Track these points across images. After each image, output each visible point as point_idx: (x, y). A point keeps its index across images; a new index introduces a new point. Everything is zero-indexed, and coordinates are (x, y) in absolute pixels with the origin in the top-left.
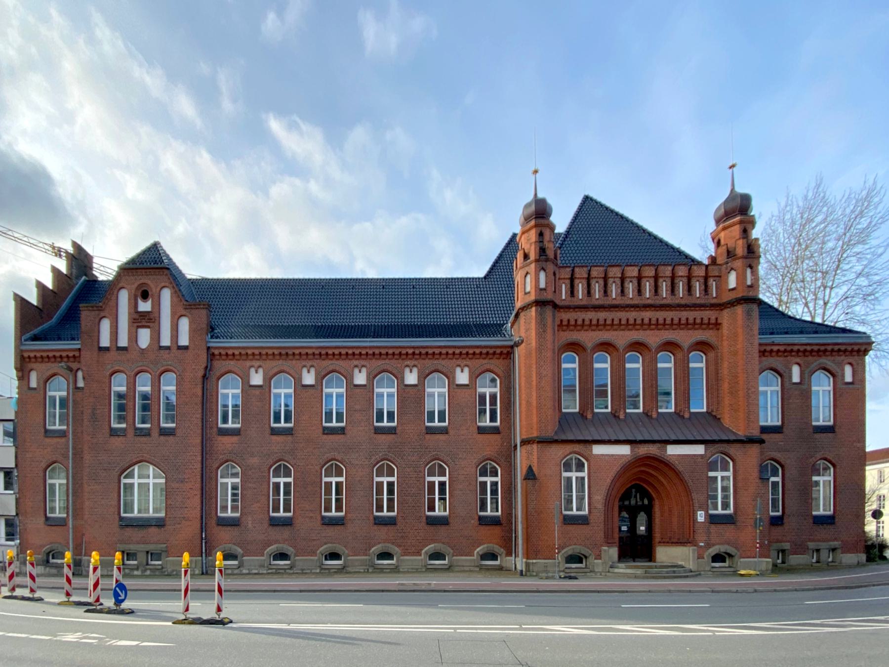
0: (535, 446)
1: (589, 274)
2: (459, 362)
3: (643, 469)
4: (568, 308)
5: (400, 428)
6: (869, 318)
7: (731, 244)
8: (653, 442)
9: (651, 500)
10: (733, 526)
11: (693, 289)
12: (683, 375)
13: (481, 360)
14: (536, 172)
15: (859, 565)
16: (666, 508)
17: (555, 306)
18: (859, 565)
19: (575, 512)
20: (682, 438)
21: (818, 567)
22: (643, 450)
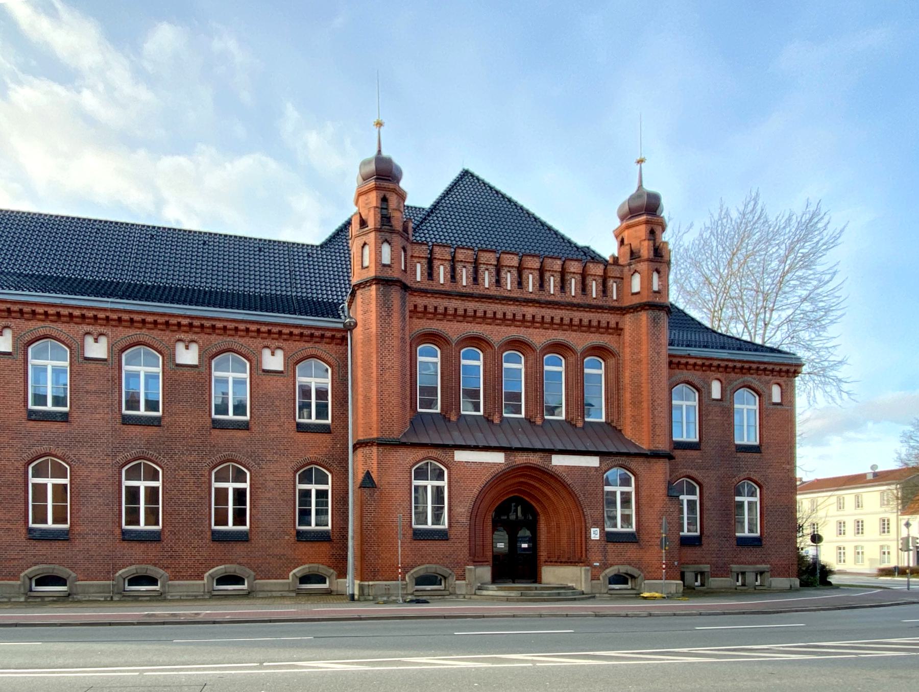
0: (374, 449)
1: (454, 258)
2: (267, 342)
3: (522, 480)
4: (424, 292)
5: (167, 419)
6: (814, 344)
7: (635, 244)
8: (534, 451)
9: (535, 515)
10: (635, 546)
11: (588, 288)
12: (577, 381)
13: (303, 344)
14: (379, 124)
15: (791, 589)
16: (553, 524)
17: (405, 287)
18: (791, 589)
19: (430, 525)
20: (570, 447)
21: (743, 591)
22: (521, 459)
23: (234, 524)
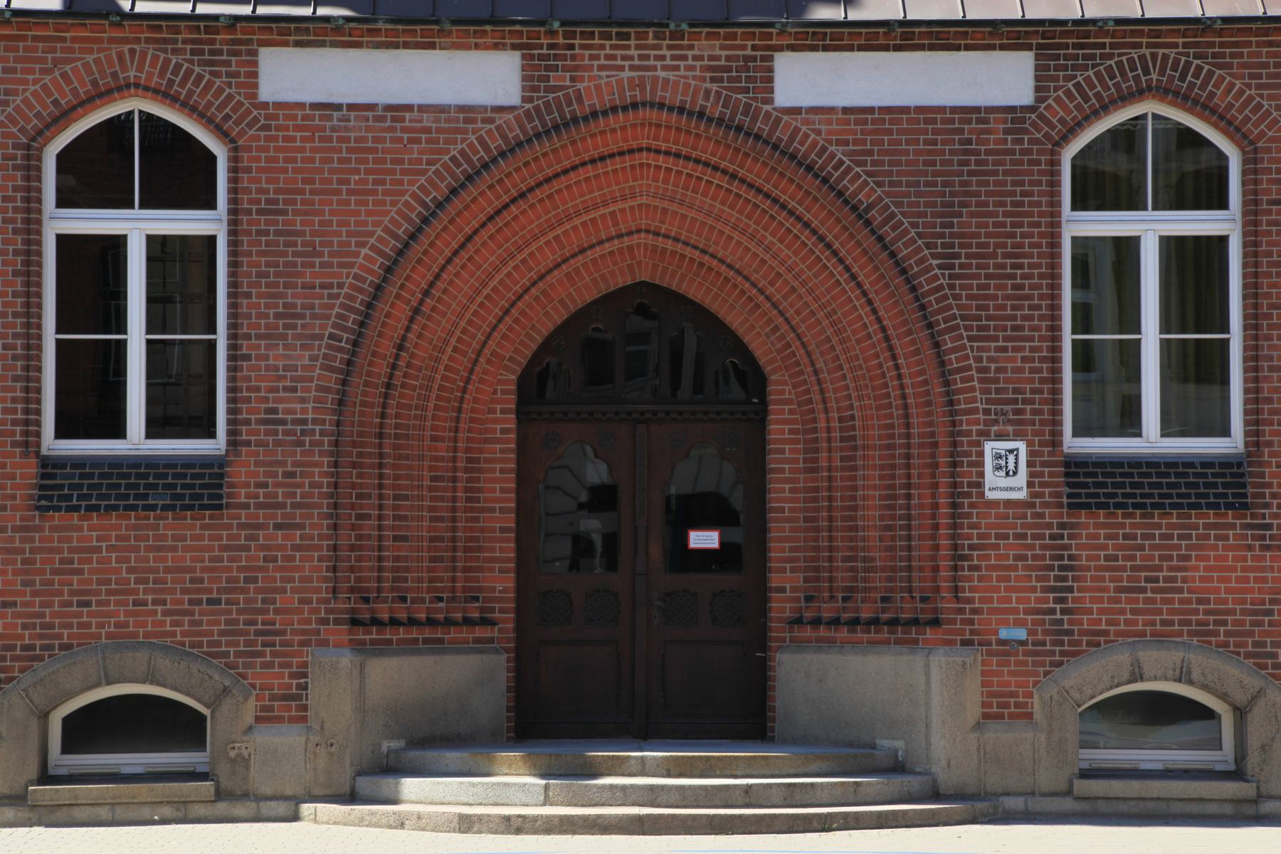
23: (1168, 429)
